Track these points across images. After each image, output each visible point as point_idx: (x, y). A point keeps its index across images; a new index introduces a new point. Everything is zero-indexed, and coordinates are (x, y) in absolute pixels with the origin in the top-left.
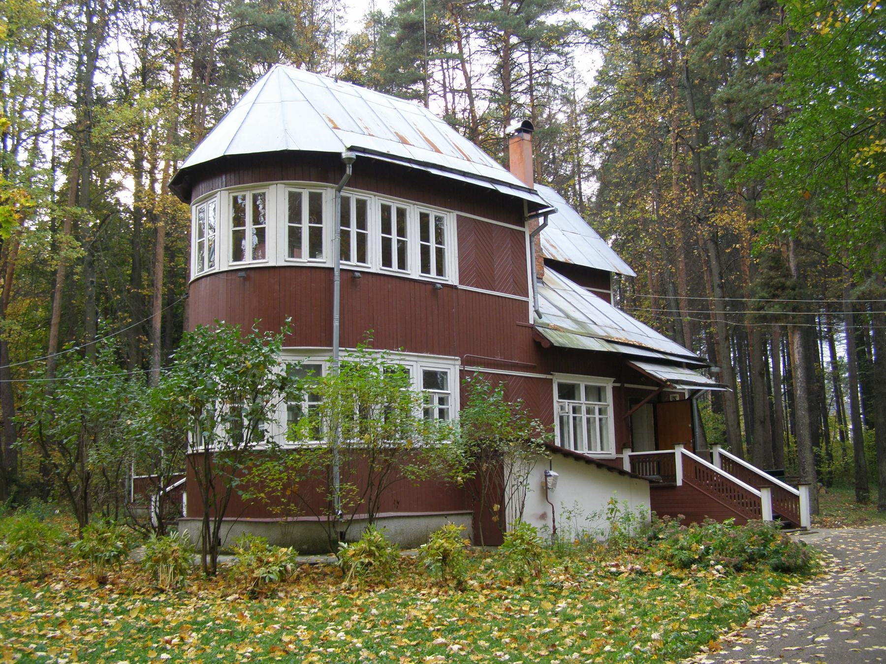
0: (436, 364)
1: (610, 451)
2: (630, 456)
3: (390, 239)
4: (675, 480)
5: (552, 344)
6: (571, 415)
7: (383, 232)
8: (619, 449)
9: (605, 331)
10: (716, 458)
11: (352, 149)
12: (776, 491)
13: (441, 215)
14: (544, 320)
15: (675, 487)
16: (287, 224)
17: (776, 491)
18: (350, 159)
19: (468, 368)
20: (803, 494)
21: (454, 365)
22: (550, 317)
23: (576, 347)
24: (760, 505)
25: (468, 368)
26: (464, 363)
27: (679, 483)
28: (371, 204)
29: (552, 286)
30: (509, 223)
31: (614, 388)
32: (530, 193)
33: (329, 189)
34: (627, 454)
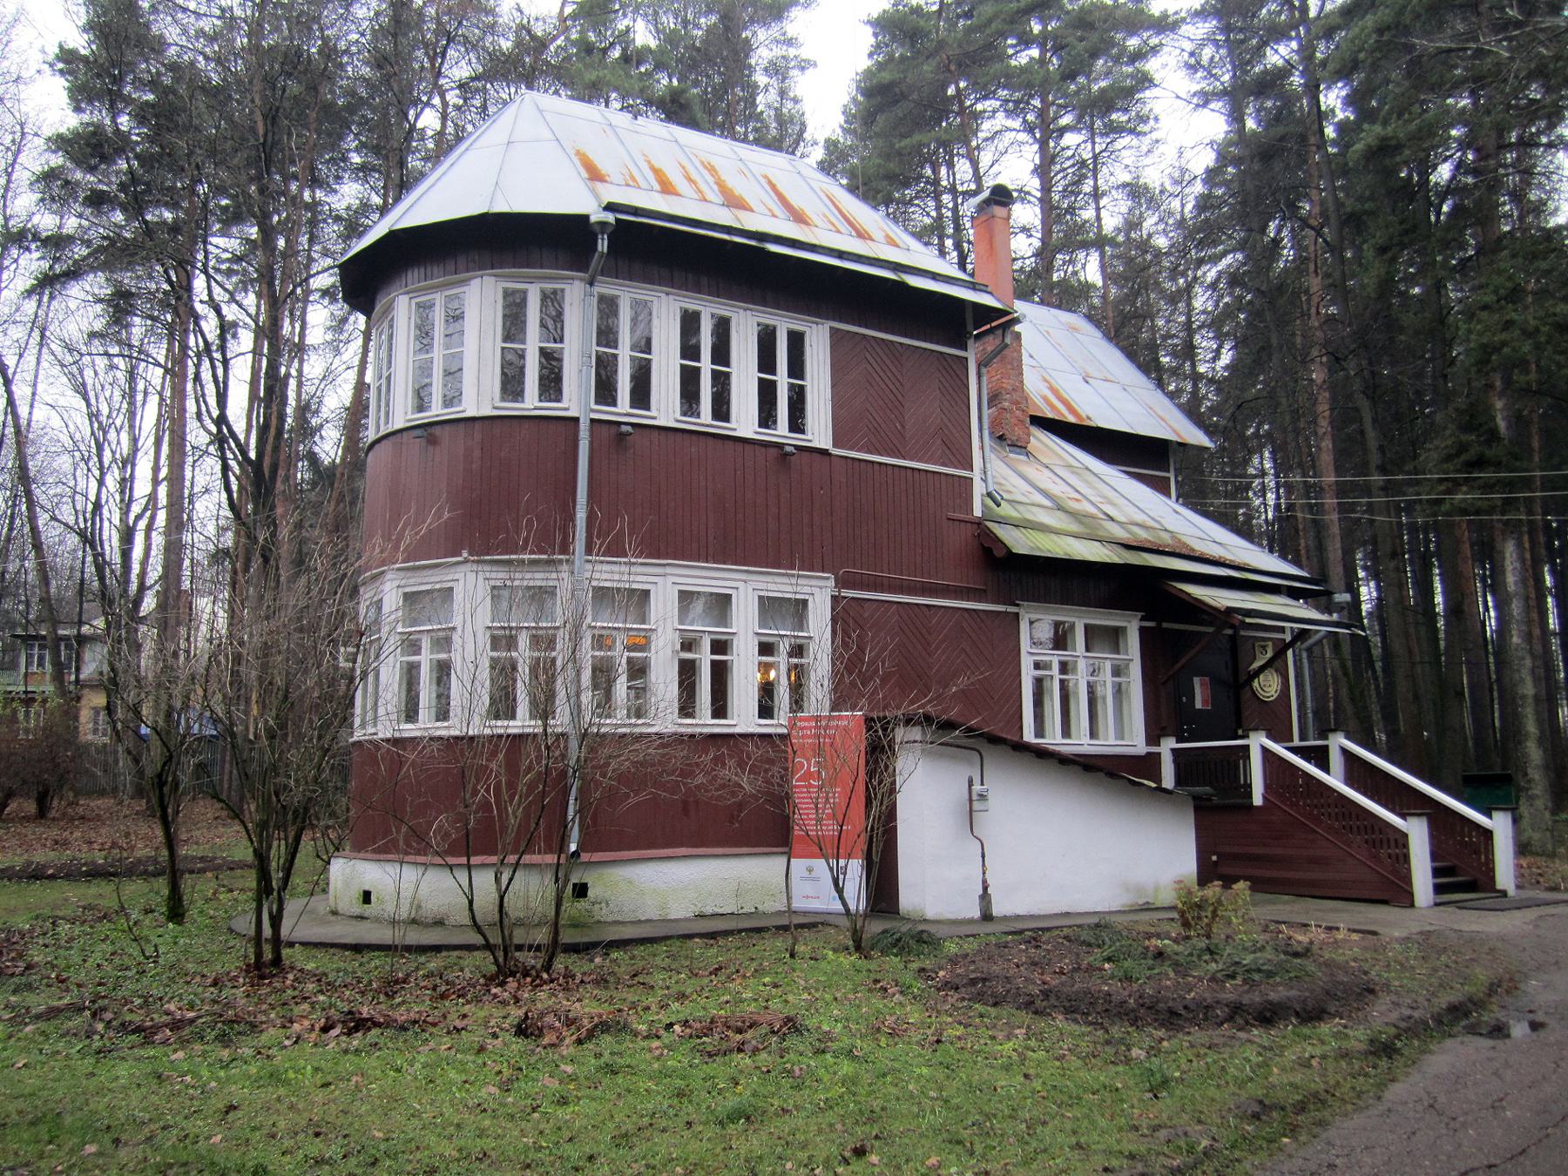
0: (781, 585)
1: (1135, 742)
2: (1173, 750)
3: (774, 383)
4: (1250, 795)
5: (1009, 552)
6: (1057, 677)
7: (760, 370)
8: (1153, 738)
9: (1129, 531)
10: (1336, 759)
11: (610, 207)
12: (1440, 819)
13: (726, 314)
14: (1006, 510)
15: (1251, 806)
16: (500, 344)
17: (1440, 819)
18: (603, 224)
19: (846, 593)
20: (1500, 825)
21: (821, 588)
22: (1034, 509)
23: (1061, 555)
24: (1406, 846)
25: (846, 593)
26: (842, 583)
27: (1257, 800)
28: (814, 338)
29: (1045, 461)
30: (938, 343)
31: (1142, 630)
32: (974, 289)
33: (577, 283)
34: (1168, 745)
